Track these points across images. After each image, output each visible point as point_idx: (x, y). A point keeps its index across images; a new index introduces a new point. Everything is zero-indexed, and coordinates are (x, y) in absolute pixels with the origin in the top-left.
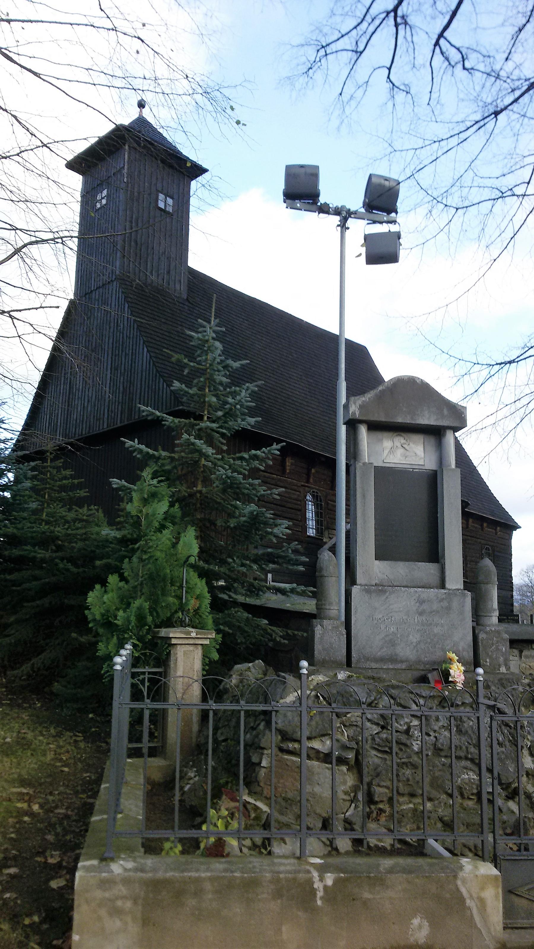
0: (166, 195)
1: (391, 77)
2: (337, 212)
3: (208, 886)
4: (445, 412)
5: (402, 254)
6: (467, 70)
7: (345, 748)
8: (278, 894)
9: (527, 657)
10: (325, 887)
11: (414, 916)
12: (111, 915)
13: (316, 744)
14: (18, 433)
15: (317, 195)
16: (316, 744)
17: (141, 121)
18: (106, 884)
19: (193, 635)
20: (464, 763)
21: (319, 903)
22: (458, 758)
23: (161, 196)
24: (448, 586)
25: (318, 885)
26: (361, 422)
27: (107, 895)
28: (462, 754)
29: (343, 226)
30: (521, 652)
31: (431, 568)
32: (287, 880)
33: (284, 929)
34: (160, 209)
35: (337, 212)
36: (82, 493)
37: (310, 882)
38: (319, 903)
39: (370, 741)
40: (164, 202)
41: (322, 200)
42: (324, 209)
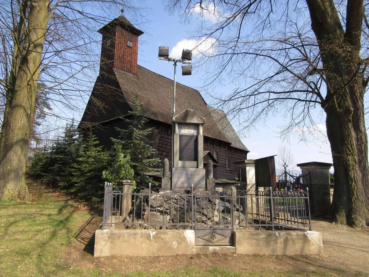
0: (130, 41)
1: (202, 6)
2: (174, 60)
3: (126, 235)
4: (199, 119)
5: (193, 72)
6: (226, 3)
7: (167, 209)
8: (142, 237)
9: (225, 188)
10: (153, 235)
11: (174, 241)
12: (103, 241)
13: (159, 208)
14: (79, 123)
15: (168, 56)
16: (159, 208)
17: (123, 17)
18: (102, 234)
19: (129, 182)
20: (198, 213)
21: (152, 238)
22: (197, 212)
23: (129, 42)
24: (199, 167)
25: (151, 235)
26: (176, 122)
27: (102, 236)
28: (198, 211)
29: (175, 64)
30: (224, 186)
31: (195, 163)
32: (144, 233)
33: (143, 244)
34: (128, 46)
35: (174, 60)
36: (97, 142)
37: (150, 234)
38: (152, 238)
39: (173, 208)
40: (130, 44)
41: (169, 57)
42: (169, 60)
